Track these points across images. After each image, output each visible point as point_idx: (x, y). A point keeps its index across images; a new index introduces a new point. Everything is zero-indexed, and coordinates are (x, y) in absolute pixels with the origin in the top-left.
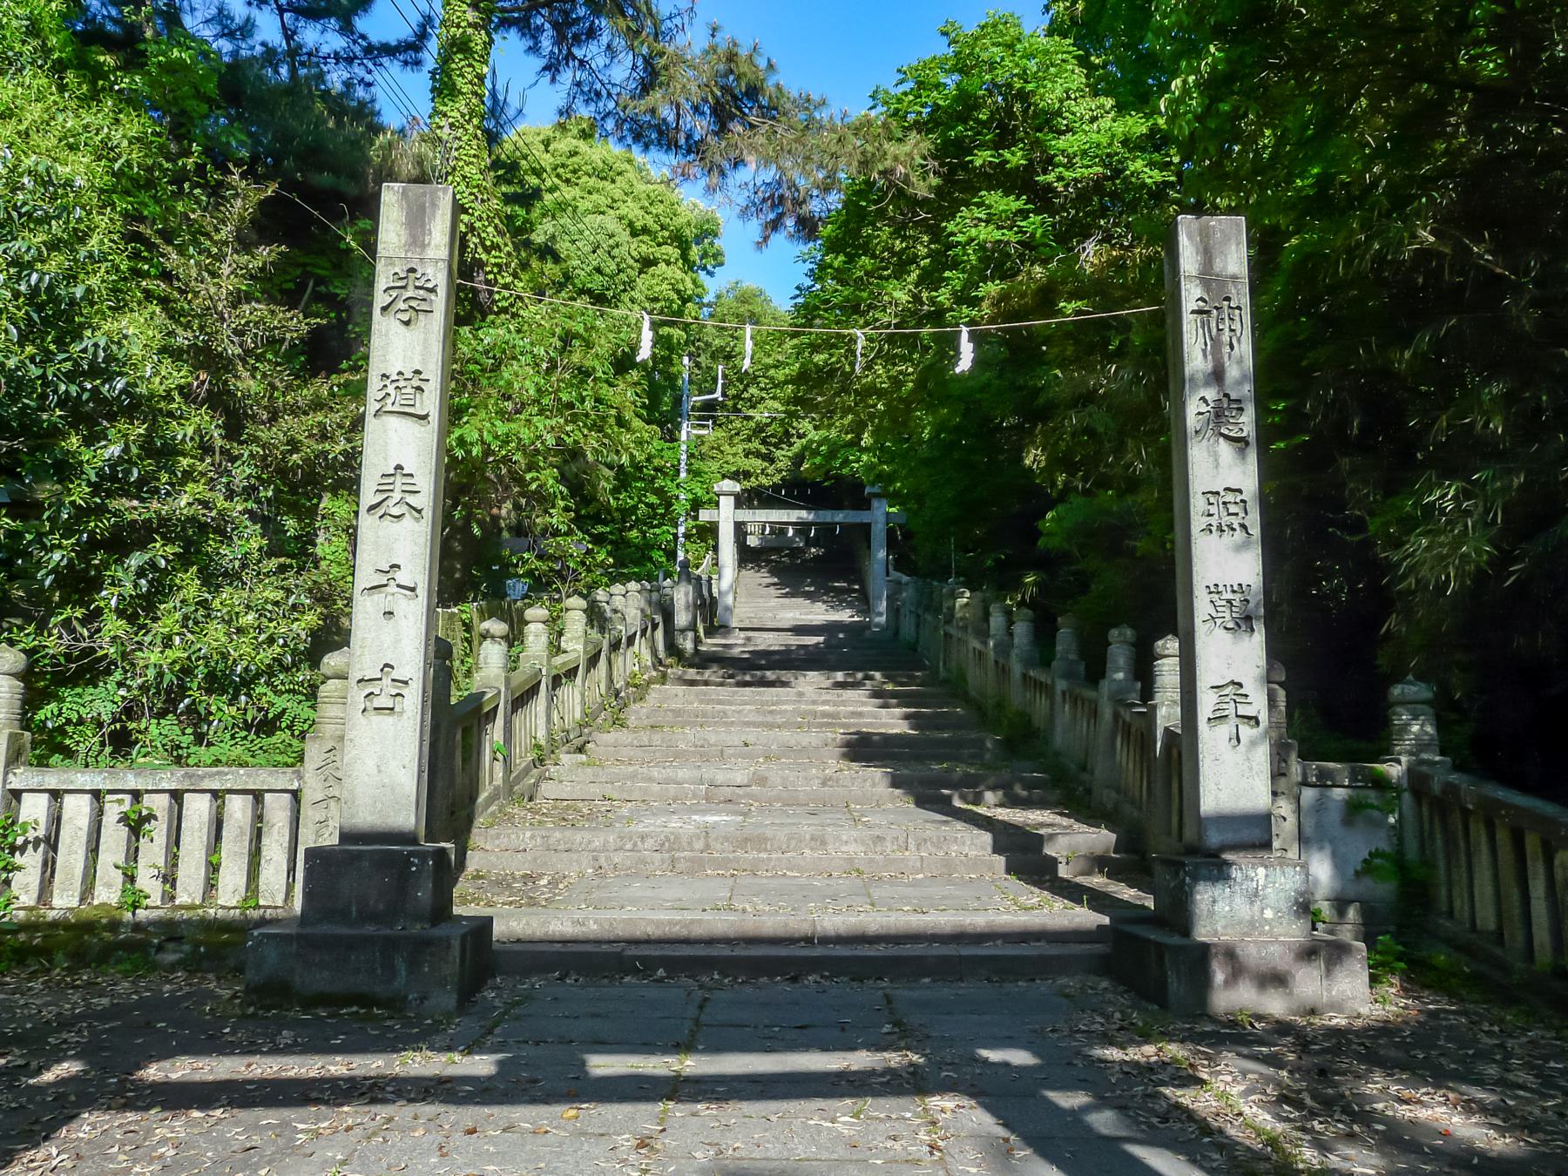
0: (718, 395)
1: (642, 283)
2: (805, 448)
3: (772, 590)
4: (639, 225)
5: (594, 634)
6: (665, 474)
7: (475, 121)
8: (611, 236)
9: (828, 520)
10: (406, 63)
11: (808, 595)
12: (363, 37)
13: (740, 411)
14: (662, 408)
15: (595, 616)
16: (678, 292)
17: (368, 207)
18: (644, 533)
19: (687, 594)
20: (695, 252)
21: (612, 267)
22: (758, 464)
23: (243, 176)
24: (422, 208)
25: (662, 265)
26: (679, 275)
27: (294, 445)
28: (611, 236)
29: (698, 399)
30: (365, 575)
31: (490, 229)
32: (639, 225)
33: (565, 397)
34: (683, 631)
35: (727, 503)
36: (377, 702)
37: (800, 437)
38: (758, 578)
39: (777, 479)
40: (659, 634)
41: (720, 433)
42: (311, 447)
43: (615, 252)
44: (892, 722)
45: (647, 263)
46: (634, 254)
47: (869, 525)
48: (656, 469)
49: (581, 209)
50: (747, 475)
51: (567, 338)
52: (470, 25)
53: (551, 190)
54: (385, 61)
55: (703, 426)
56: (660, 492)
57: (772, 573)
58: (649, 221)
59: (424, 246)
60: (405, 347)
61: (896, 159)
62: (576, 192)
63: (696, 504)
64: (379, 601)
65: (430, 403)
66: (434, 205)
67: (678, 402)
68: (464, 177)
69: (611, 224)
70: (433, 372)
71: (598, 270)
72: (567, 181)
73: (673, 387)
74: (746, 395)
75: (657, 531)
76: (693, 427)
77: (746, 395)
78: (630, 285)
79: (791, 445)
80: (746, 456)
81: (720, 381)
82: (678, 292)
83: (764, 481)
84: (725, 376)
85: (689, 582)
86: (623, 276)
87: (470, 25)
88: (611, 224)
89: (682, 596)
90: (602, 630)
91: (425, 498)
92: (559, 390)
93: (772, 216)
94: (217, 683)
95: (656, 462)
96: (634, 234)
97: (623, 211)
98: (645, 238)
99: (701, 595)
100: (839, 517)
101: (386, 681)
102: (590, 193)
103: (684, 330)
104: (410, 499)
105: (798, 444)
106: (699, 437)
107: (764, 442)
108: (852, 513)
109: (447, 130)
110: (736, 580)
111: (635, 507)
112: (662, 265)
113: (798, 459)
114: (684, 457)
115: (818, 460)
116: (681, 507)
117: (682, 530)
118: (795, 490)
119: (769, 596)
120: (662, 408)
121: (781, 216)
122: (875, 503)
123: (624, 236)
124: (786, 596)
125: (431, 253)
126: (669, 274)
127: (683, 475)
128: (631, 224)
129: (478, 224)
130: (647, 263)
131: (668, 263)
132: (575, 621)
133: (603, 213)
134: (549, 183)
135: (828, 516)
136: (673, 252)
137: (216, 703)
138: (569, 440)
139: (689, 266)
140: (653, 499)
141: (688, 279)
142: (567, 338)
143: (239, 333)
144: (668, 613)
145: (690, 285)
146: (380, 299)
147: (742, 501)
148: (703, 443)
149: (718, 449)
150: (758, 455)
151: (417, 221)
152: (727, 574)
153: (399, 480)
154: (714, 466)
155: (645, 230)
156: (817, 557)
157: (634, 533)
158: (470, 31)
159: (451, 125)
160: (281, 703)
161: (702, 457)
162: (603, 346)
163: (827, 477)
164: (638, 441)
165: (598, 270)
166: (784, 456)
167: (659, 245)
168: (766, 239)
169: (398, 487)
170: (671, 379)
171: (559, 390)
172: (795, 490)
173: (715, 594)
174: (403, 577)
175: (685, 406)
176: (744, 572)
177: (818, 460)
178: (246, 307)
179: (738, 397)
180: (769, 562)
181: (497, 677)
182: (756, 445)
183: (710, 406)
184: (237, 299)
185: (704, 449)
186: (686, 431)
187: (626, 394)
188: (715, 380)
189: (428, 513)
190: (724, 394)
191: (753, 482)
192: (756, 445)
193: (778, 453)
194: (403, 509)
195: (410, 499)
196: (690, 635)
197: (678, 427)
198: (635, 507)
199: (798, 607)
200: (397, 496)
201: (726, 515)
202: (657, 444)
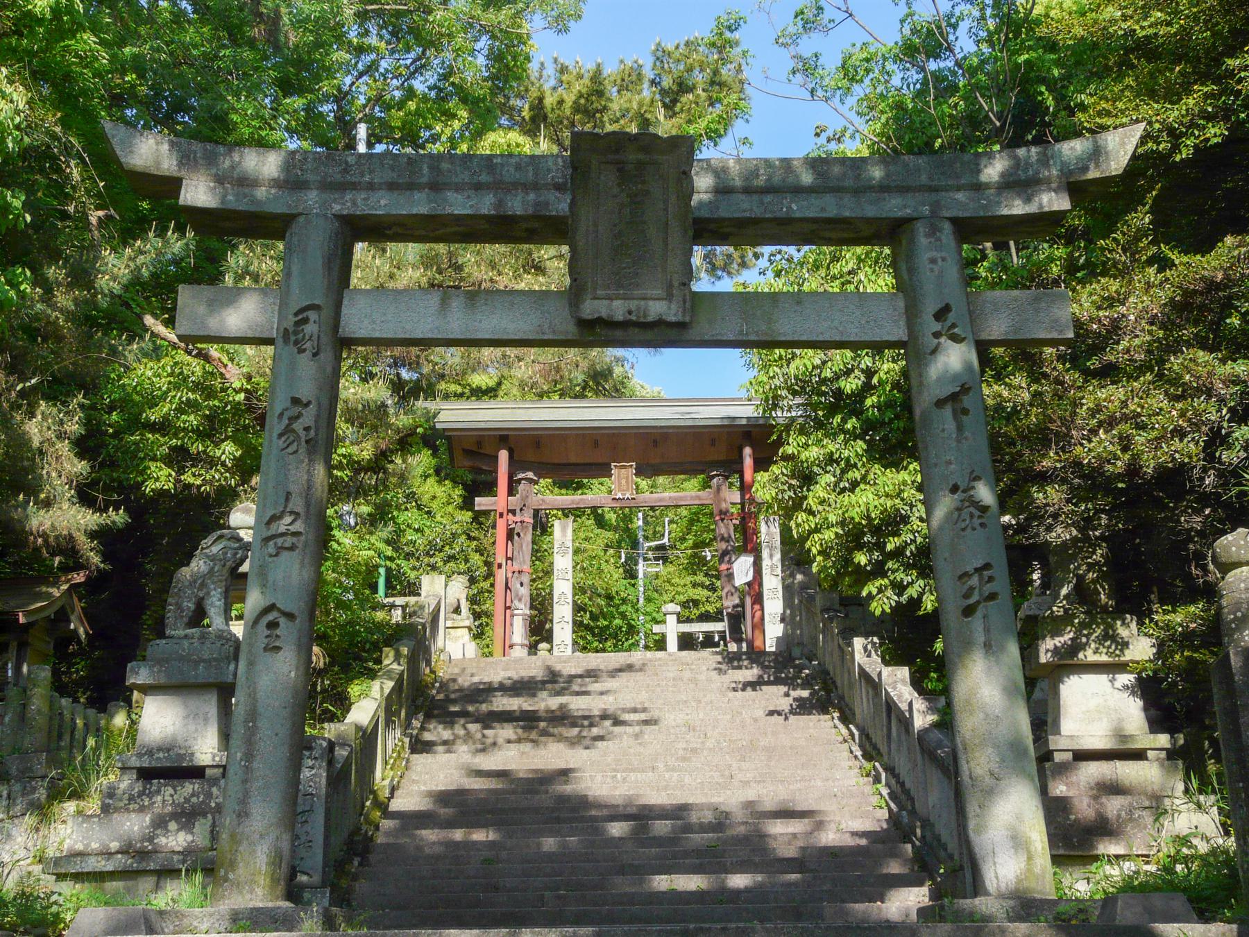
35: (671, 620)
41: (671, 568)
50: (696, 603)
107: (706, 575)
127: (642, 600)
150: (702, 585)
151: (564, 529)
192: (700, 578)
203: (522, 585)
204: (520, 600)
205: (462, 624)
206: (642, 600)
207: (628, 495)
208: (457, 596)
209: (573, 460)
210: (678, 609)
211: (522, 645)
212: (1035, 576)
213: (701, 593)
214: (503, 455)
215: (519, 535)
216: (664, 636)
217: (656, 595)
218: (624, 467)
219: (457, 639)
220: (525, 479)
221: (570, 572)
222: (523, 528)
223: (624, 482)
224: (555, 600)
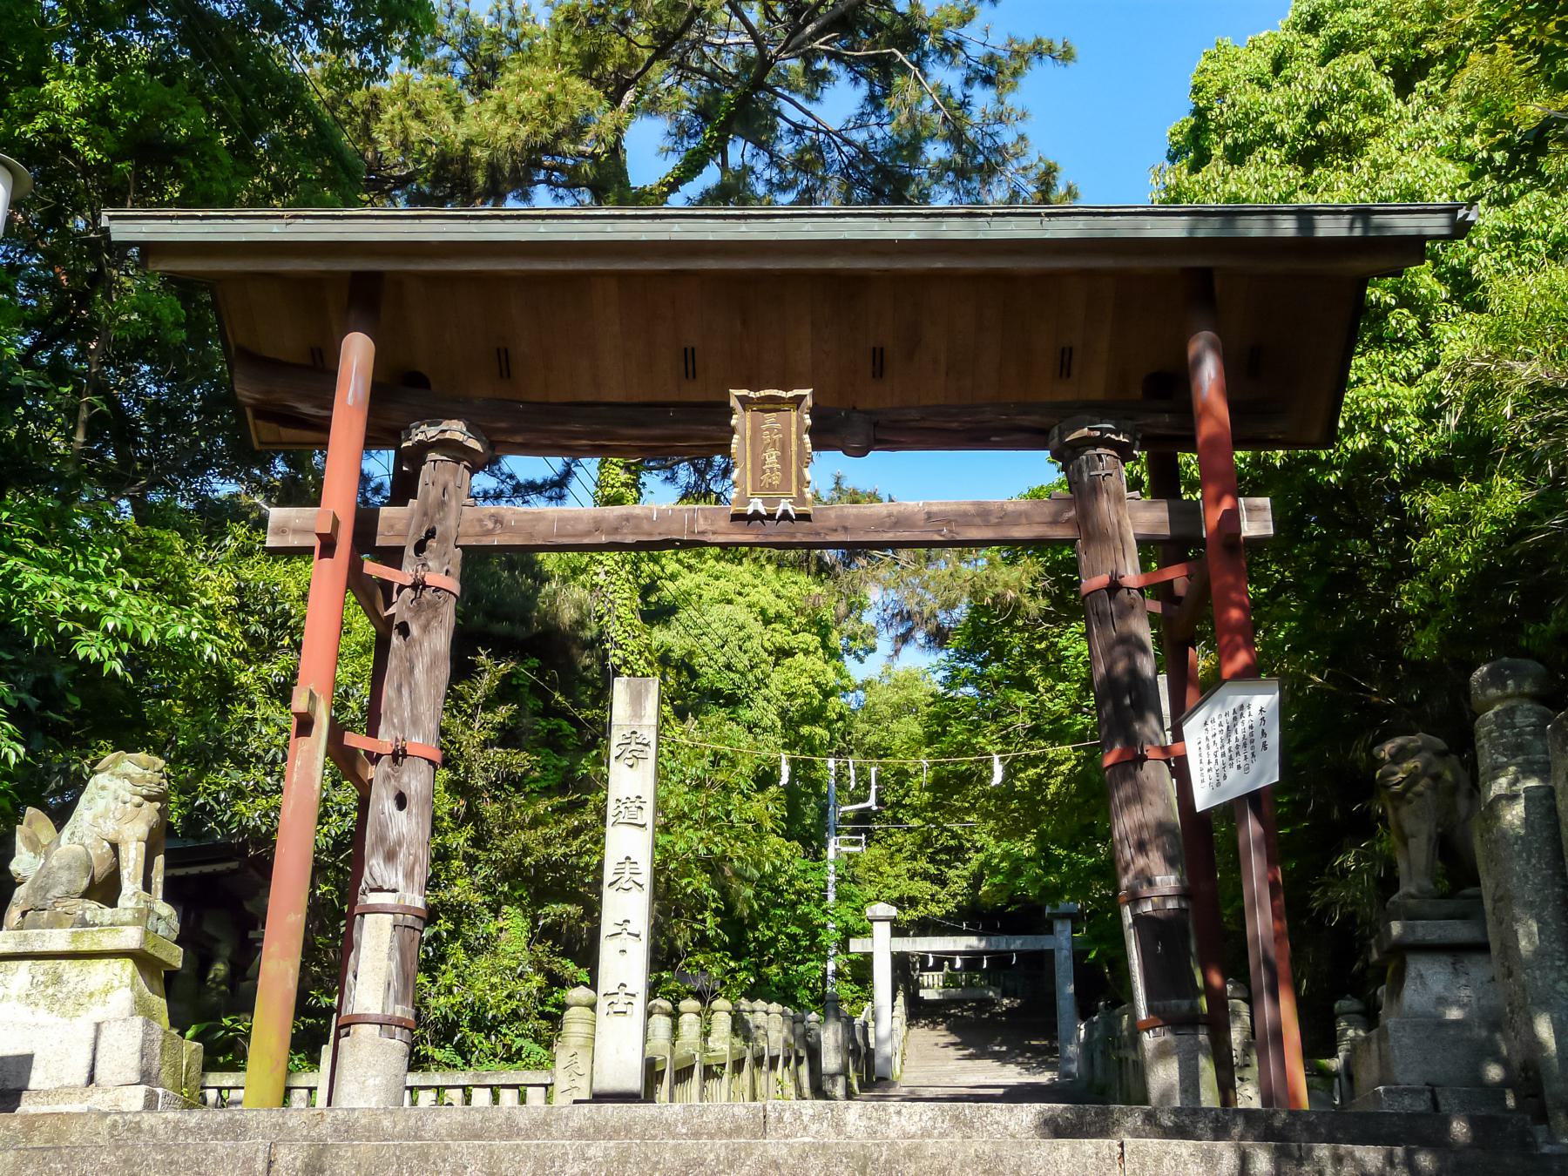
0: (871, 803)
1: (776, 678)
2: (985, 864)
3: (951, 1051)
4: (771, 612)
5: (739, 1043)
6: (808, 899)
7: (628, 567)
8: (741, 628)
9: (1003, 947)
10: (551, 498)
11: (998, 1057)
12: (511, 477)
13: (900, 821)
14: (805, 824)
15: (740, 1026)
16: (818, 685)
17: (602, 696)
18: (785, 971)
19: (836, 1033)
20: (836, 640)
21: (742, 662)
22: (927, 887)
23: (488, 656)
24: (640, 693)
25: (800, 657)
26: (820, 665)
27: (526, 851)
28: (741, 628)
29: (850, 809)
30: (607, 927)
31: (641, 662)
32: (771, 612)
33: (712, 812)
34: (833, 1076)
35: (882, 930)
36: (617, 1008)
37: (978, 851)
38: (932, 1038)
39: (951, 906)
40: (804, 1070)
41: (877, 850)
42: (540, 852)
43: (748, 644)
44: (958, 1040)
45: (783, 653)
46: (767, 644)
47: (1052, 952)
48: (799, 893)
49: (706, 596)
50: (913, 902)
51: (717, 759)
52: (623, 484)
53: (673, 577)
54: (533, 497)
55: (857, 843)
56: (804, 921)
57: (952, 1029)
58: (782, 606)
59: (641, 717)
60: (629, 782)
61: (1006, 585)
62: (701, 578)
63: (848, 933)
64: (616, 943)
65: (647, 816)
66: (647, 690)
67: (824, 812)
68: (618, 618)
69: (741, 614)
70: (649, 797)
71: (728, 667)
72: (690, 568)
73: (818, 794)
74: (907, 801)
75: (801, 968)
76: (844, 843)
77: (907, 801)
78: (762, 683)
79: (965, 861)
80: (911, 878)
81: (874, 787)
82: (818, 685)
83: (935, 909)
84: (879, 780)
85: (838, 1019)
86: (758, 672)
87: (623, 484)
88: (741, 614)
89: (830, 1037)
90: (747, 1039)
91: (645, 878)
92: (707, 805)
93: (902, 630)
94: (477, 1024)
95: (798, 884)
96: (767, 622)
97: (753, 598)
98: (777, 626)
99: (854, 1040)
100: (1017, 943)
101: (622, 995)
102: (717, 578)
103: (827, 728)
104: (635, 878)
105: (976, 859)
106: (850, 856)
107: (932, 860)
108: (1030, 938)
109: (602, 576)
110: (905, 1039)
111: (774, 940)
112: (800, 657)
113: (976, 880)
114: (832, 878)
115: (998, 879)
116: (830, 936)
117: (831, 966)
118: (971, 917)
119: (947, 1058)
120: (805, 824)
121: (910, 630)
122: (1058, 926)
123: (756, 627)
124: (970, 1057)
125: (645, 721)
126: (809, 666)
127: (831, 897)
128: (763, 612)
129: (631, 658)
130: (783, 653)
131: (806, 652)
132: (722, 1023)
133: (730, 602)
134: (668, 571)
135: (1002, 943)
136: (811, 640)
137: (477, 1038)
138: (716, 850)
139: (833, 654)
140: (793, 929)
141: (830, 669)
142: (717, 759)
143: (485, 770)
144: (814, 1054)
145: (831, 675)
146: (614, 751)
147: (898, 930)
148: (856, 864)
149: (876, 870)
150: (926, 876)
151: (637, 700)
152: (885, 1015)
153: (628, 866)
154: (871, 892)
155: (779, 617)
156: (1010, 1011)
157: (774, 969)
158: (623, 490)
159: (607, 573)
160: (519, 1042)
161: (854, 880)
162: (746, 767)
163: (1012, 900)
164: (780, 851)
165: (728, 667)
166: (958, 877)
167: (795, 633)
168: (897, 652)
169: (627, 871)
170: (816, 784)
171: (707, 805)
172: (971, 917)
173: (872, 1046)
174: (631, 928)
175: (831, 817)
176: (915, 1030)
177: (998, 879)
178: (490, 751)
179: (899, 804)
180: (946, 1017)
181: (663, 1047)
182: (922, 864)
183: (864, 817)
184: (486, 744)
185: (858, 871)
186: (834, 848)
187: (765, 807)
188: (868, 785)
189: (647, 887)
190: (880, 802)
191: (921, 911)
192: (922, 864)
193: (951, 873)
194: (630, 884)
195: (635, 878)
196: (841, 1080)
197: (824, 844)
198: (774, 940)
199: (984, 1070)
200: (627, 876)
201: (881, 946)
202: (799, 863)
203: (401, 801)
204: (390, 857)
205: (109, 942)
206: (831, 897)
207: (784, 505)
208: (109, 829)
209: (614, 393)
210: (893, 911)
211: (385, 1023)
212: (985, 888)
213: (922, 888)
214: (357, 354)
215: (404, 630)
216: (868, 957)
217: (854, 889)
218: (773, 404)
219: (81, 1001)
220: (444, 445)
221: (649, 808)
222: (418, 607)
223: (771, 457)
224: (608, 876)
